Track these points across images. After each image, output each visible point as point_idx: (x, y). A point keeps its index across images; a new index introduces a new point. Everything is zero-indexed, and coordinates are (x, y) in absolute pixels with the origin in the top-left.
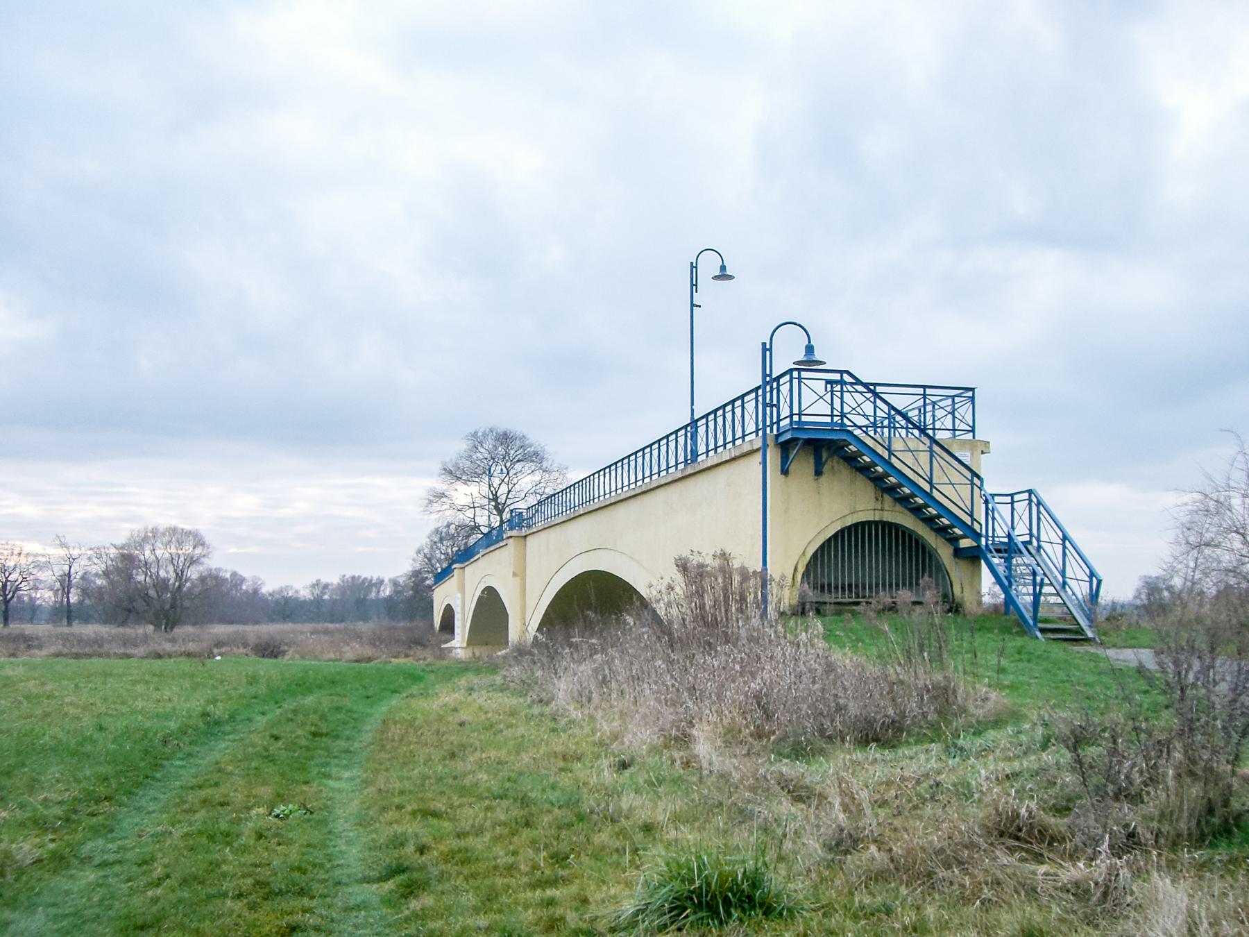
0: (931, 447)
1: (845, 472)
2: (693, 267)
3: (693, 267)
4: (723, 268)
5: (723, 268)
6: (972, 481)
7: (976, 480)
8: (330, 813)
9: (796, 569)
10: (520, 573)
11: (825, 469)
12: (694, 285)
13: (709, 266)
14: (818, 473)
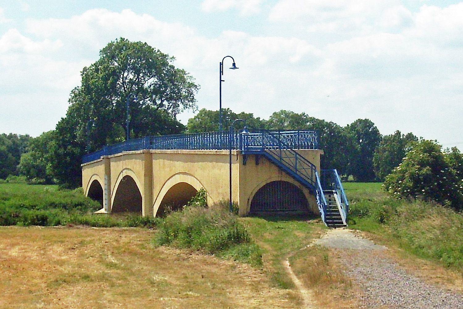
0: (296, 156)
1: (267, 163)
2: (221, 64)
3: (221, 64)
4: (234, 64)
5: (234, 64)
6: (312, 167)
7: (314, 167)
8: (205, 207)
9: (249, 199)
10: (108, 172)
11: (260, 162)
12: (221, 72)
13: (228, 63)
14: (257, 164)
